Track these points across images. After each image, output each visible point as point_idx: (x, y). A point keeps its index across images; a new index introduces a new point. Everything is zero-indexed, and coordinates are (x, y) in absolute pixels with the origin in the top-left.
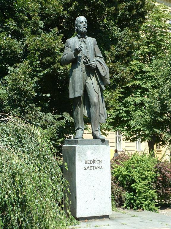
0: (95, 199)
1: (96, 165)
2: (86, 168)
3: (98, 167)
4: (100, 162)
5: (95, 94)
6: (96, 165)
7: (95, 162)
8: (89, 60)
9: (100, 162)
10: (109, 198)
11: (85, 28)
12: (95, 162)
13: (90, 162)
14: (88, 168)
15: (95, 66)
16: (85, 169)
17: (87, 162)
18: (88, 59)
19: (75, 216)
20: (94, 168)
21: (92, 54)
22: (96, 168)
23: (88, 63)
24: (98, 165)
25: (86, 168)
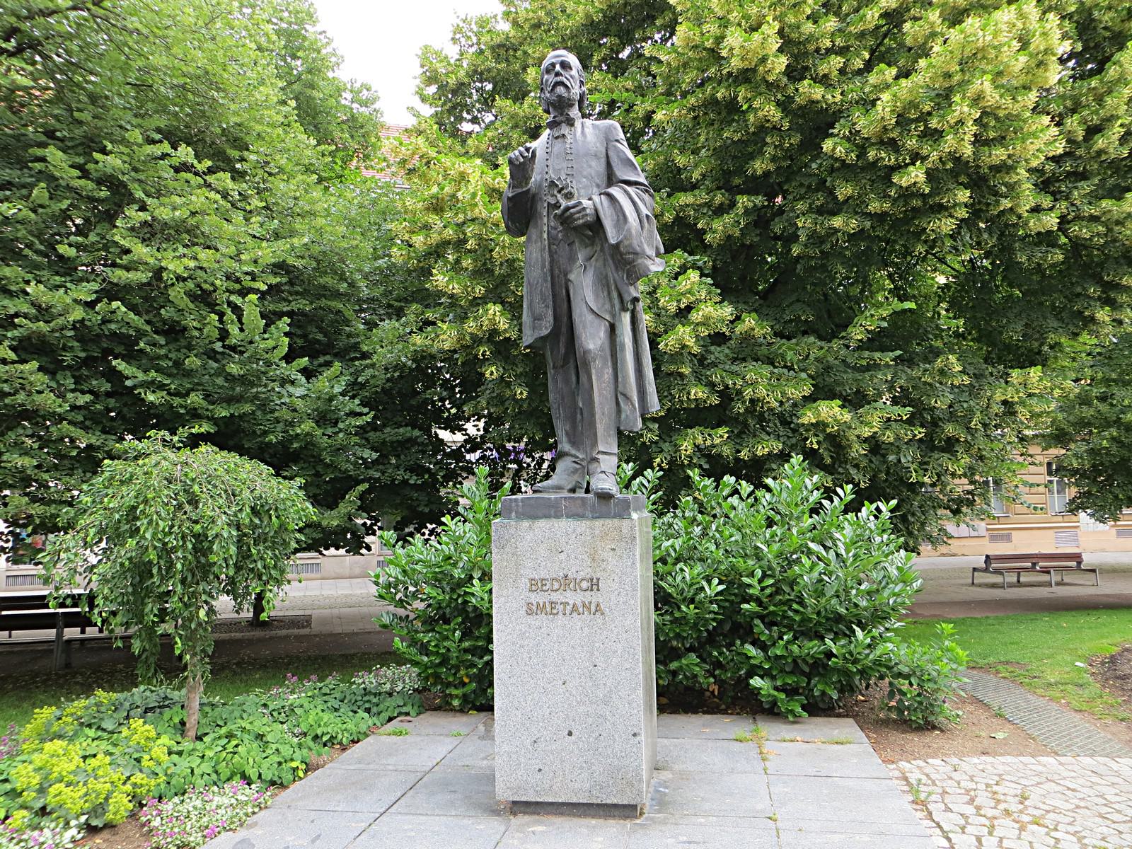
0: (570, 734)
1: (572, 598)
16: (530, 612)
20: (569, 608)
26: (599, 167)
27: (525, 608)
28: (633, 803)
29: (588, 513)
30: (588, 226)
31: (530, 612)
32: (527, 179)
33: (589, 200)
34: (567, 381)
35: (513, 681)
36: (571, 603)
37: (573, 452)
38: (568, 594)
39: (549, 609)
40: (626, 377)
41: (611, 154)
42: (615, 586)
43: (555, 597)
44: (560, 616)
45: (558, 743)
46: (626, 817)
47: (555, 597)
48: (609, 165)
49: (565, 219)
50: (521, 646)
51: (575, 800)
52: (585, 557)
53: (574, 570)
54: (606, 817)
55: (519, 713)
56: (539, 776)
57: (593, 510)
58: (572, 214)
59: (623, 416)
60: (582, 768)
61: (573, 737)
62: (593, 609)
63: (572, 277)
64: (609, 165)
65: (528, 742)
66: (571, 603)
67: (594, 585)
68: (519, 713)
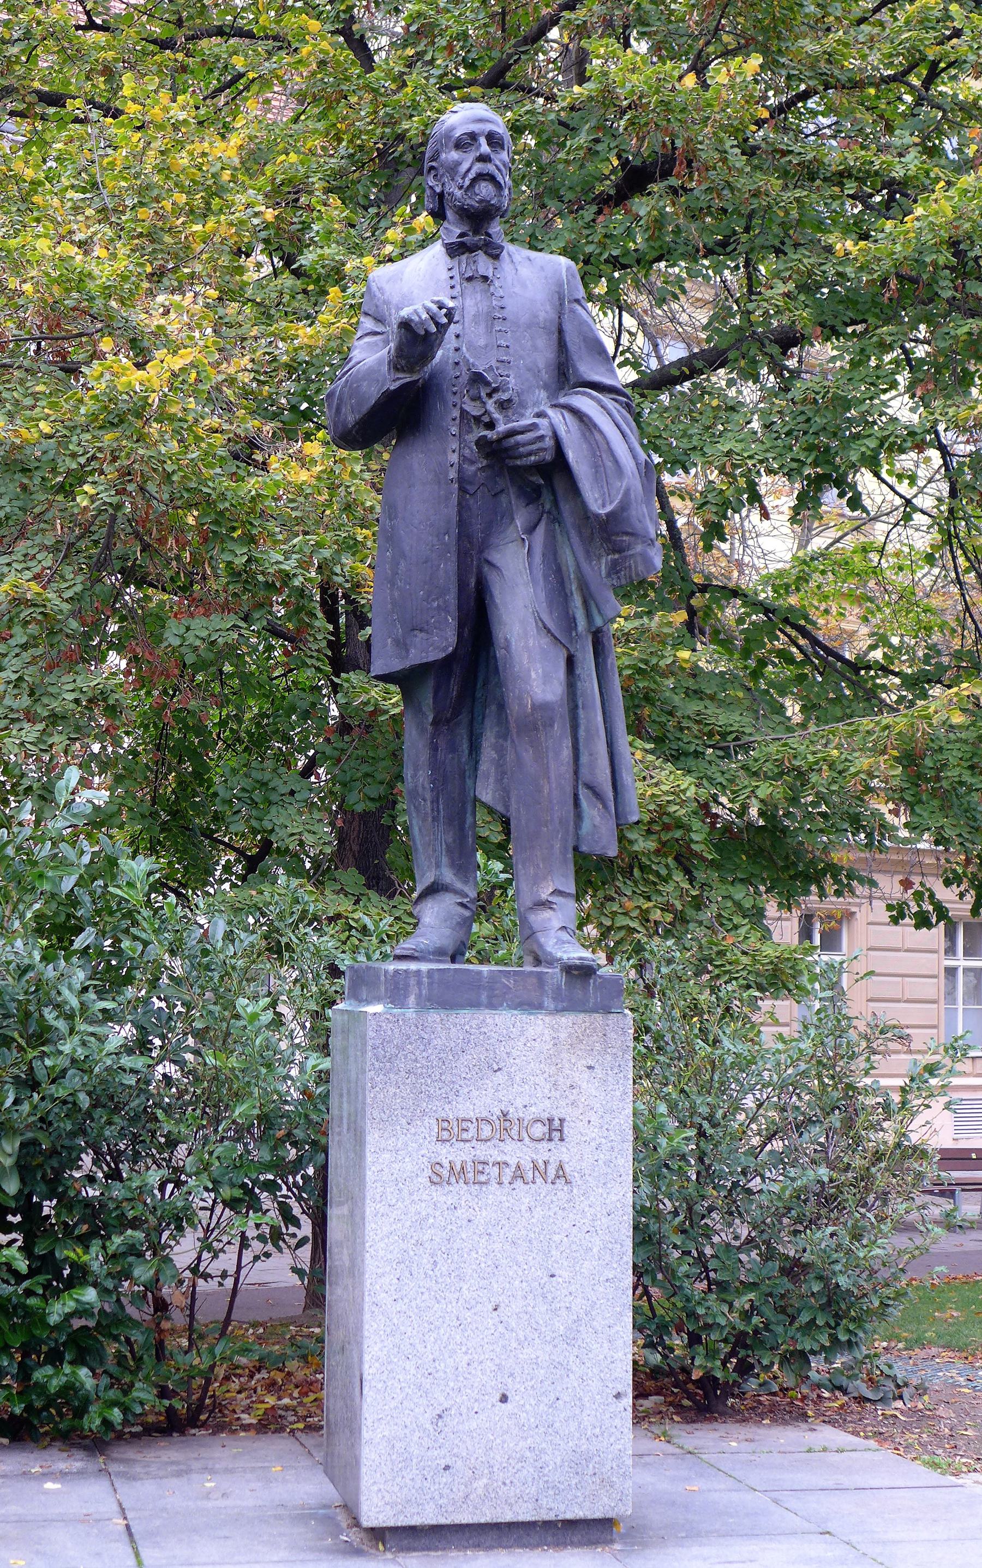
0: (504, 1399)
1: (516, 1153)
2: (445, 1173)
3: (535, 1167)
4: (556, 1135)
5: (735, 1496)
6: (516, 1153)
7: (514, 1133)
8: (503, 406)
9: (556, 1135)
10: (618, 1396)
11: (483, 184)
12: (514, 1133)
13: (472, 1133)
14: (458, 1173)
15: (549, 442)
16: (436, 1180)
17: (450, 1131)
18: (496, 397)
19: (477, 527)
20: (508, 1172)
21: (64, 1460)
22: (519, 1174)
23: (491, 425)
24: (543, 1152)
25: (445, 1173)
26: (542, 354)
27: (428, 1172)
28: (609, 1515)
29: (548, 1003)
30: (540, 468)
31: (436, 1180)
32: (427, 356)
33: (542, 418)
34: (453, 748)
35: (400, 1306)
36: (513, 1162)
37: (459, 885)
38: (509, 1146)
39: (470, 1175)
40: (592, 765)
41: (567, 327)
42: (593, 1132)
43: (483, 1151)
44: (494, 1186)
45: (482, 1416)
46: (592, 1543)
47: (483, 1151)
48: (562, 345)
49: (498, 453)
50: (419, 1243)
51: (508, 1517)
52: (540, 1080)
53: (519, 1103)
54: (559, 1544)
55: (411, 1366)
56: (446, 1478)
57: (557, 997)
58: (518, 445)
59: (586, 826)
60: (522, 1459)
61: (508, 1407)
62: (552, 1172)
63: (495, 557)
64: (562, 345)
65: (426, 1420)
66: (513, 1162)
67: (555, 1129)
68: (411, 1366)
